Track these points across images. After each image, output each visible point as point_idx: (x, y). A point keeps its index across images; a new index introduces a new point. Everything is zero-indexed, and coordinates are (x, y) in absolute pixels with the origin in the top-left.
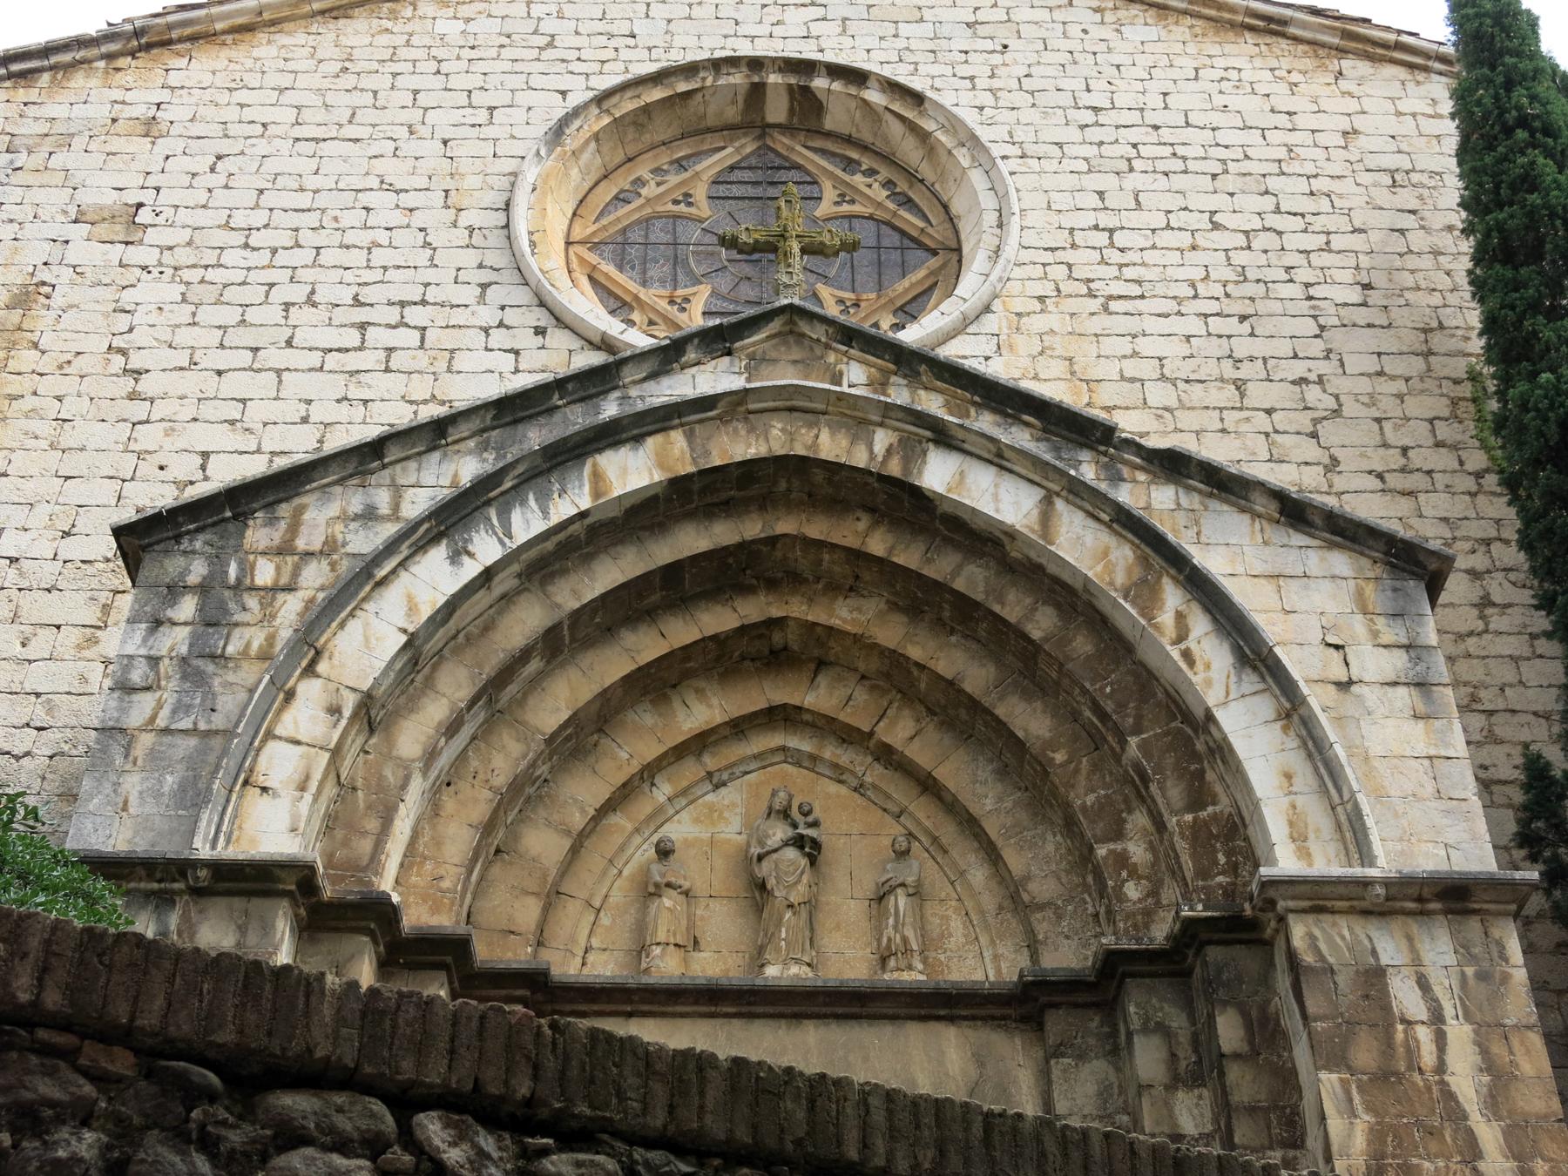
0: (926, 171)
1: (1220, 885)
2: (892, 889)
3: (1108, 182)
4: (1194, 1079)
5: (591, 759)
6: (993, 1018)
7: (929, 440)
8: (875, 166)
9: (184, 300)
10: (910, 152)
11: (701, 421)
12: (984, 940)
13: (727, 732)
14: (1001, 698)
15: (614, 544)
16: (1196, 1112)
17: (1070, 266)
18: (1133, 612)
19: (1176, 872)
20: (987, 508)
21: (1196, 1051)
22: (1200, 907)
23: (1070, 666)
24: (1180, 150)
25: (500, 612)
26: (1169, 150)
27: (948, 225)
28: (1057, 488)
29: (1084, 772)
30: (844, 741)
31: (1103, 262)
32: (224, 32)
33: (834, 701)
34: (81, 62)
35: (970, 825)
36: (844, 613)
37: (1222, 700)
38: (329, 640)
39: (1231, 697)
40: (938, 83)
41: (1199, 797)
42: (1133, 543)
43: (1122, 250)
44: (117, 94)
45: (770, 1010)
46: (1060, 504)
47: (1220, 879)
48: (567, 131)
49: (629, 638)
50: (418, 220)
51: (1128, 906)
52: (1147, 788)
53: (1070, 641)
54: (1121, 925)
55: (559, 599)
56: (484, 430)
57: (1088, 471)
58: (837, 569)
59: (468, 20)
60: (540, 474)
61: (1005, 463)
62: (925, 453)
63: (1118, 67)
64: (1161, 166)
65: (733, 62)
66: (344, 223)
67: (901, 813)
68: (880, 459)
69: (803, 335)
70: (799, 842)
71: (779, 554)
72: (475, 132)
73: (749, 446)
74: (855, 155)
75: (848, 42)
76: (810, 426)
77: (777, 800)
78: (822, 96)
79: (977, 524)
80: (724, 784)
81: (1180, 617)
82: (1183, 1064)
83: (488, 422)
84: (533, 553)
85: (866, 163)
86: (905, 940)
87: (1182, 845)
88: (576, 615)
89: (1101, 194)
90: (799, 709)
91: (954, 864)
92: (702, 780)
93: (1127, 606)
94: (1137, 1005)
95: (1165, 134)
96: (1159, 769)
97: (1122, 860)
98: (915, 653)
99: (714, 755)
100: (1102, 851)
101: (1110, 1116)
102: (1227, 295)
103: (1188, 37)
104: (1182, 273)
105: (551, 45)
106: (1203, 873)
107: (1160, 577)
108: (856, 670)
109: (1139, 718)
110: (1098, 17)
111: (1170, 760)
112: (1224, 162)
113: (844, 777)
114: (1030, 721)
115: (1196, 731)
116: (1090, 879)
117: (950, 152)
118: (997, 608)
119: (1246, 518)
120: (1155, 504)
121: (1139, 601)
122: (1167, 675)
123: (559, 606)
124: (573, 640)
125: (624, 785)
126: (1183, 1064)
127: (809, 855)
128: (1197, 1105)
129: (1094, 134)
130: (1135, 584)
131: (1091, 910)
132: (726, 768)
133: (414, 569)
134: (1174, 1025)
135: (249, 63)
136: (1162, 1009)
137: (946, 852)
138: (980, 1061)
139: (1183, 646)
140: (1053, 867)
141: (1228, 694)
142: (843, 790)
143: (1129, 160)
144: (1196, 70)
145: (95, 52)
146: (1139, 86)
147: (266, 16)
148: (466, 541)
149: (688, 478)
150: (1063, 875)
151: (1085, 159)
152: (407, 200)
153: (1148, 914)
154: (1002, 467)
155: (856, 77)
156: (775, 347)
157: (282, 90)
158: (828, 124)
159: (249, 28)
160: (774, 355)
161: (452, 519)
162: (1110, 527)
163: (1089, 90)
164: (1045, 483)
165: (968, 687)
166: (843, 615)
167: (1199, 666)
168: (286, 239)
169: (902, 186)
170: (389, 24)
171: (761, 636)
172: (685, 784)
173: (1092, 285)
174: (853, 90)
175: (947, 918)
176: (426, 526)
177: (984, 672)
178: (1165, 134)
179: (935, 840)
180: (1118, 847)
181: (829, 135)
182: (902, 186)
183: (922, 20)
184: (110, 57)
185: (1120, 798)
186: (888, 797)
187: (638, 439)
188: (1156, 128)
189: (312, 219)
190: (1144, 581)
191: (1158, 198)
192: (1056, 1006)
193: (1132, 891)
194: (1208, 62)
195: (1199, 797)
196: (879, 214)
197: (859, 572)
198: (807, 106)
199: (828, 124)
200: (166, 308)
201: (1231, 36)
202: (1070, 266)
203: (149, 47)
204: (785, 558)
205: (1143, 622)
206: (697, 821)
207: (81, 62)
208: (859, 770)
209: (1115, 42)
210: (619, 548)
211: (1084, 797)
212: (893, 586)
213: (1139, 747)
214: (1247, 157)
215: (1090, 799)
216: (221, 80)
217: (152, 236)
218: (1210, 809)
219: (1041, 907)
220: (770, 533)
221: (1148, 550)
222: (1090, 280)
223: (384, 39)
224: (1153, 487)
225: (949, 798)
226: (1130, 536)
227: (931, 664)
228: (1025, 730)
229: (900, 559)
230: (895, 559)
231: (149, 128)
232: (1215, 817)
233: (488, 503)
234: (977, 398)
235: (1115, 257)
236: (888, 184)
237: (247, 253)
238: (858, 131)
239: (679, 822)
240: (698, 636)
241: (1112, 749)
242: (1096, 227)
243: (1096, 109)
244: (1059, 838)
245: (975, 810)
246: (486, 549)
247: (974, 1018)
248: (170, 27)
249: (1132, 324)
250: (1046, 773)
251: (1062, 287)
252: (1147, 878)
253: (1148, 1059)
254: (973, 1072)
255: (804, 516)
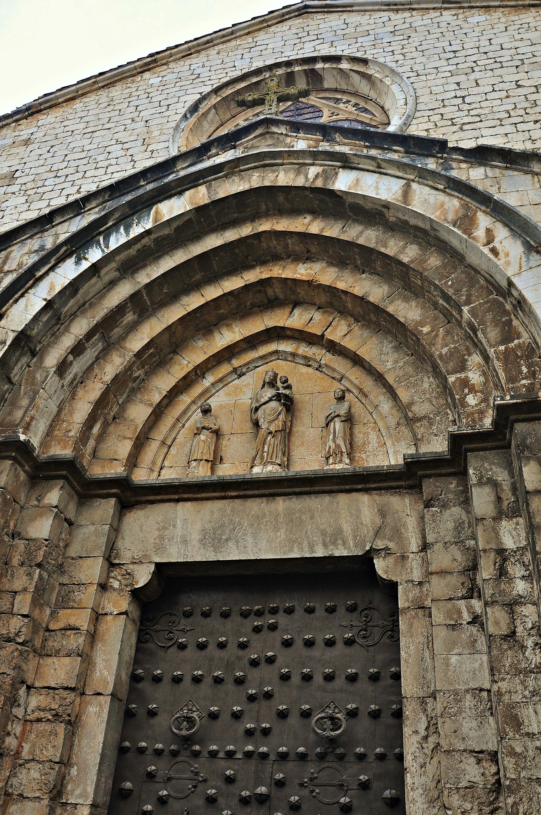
0: (373, 95)
1: (524, 385)
2: (333, 419)
3: (462, 78)
4: (514, 513)
5: (168, 367)
6: (391, 488)
7: (339, 167)
8: (349, 99)
9: (27, 202)
10: (364, 87)
11: (215, 179)
12: (389, 444)
13: (244, 346)
14: (391, 302)
15: (172, 250)
16: (514, 533)
17: (442, 115)
18: (459, 232)
19: (498, 386)
20: (372, 194)
21: (514, 493)
22: (508, 397)
23: (426, 274)
24: (498, 60)
25: (108, 291)
26: (494, 60)
27: (384, 115)
28: (412, 177)
29: (441, 336)
30: (310, 344)
31: (460, 110)
32: (63, 102)
33: (302, 321)
34: (6, 125)
35: (379, 378)
36: (303, 271)
37: (517, 271)
38: (8, 309)
39: (523, 270)
40: (375, 56)
41: (508, 334)
42: (458, 197)
43: (469, 104)
44: (17, 133)
45: (256, 492)
46: (414, 186)
47: (524, 382)
48: (201, 106)
49: (185, 300)
50: (130, 152)
51: (469, 410)
52: (476, 336)
53: (427, 261)
54: (464, 421)
55: (139, 280)
56: (103, 203)
57: (431, 164)
58: (297, 248)
59: (163, 77)
60: (129, 216)
61: (382, 170)
62: (337, 174)
63: (466, 34)
64: (488, 67)
65: (277, 65)
66: (98, 160)
67: (342, 378)
68: (311, 180)
69: (274, 133)
70: (278, 397)
71: (264, 244)
72: (160, 115)
73: (240, 186)
74: (339, 96)
75: (334, 49)
76: (274, 171)
77: (267, 377)
78: (320, 72)
79: (368, 206)
80: (244, 374)
81: (489, 231)
82: (506, 503)
83: (106, 198)
84: (123, 256)
85: (345, 98)
86: (338, 446)
87: (498, 365)
88: (147, 286)
89: (458, 84)
90: (283, 328)
91: (372, 402)
92: (231, 373)
93: (456, 230)
94: (475, 469)
95: (490, 55)
96: (482, 322)
97: (465, 383)
98: (341, 285)
99: (238, 359)
100: (451, 379)
101: (462, 542)
102: (527, 113)
103: (501, 15)
104: (502, 108)
105: (198, 77)
106: (511, 379)
107: (476, 212)
108: (315, 304)
109: (469, 296)
110: (455, 17)
111: (489, 316)
112: (522, 60)
113: (310, 363)
114: (408, 312)
115: (505, 298)
116: (449, 400)
117: (381, 81)
118: (383, 250)
119: (529, 176)
120: (471, 178)
121: (463, 226)
122: (483, 266)
123: (139, 283)
124: (153, 303)
125: (184, 378)
126: (506, 503)
127: (284, 405)
128: (516, 529)
129: (455, 61)
130: (460, 218)
131: (451, 418)
132: (244, 365)
133: (58, 270)
134: (500, 479)
135: (71, 111)
136: (491, 469)
137: (367, 396)
138: (382, 513)
139: (491, 246)
140: (428, 396)
141: (521, 268)
142: (310, 370)
143: (472, 68)
144: (506, 27)
145: (11, 120)
146: (477, 39)
147: (80, 92)
148: (85, 253)
149: (206, 206)
150: (434, 400)
151: (449, 71)
152: (126, 146)
153: (482, 413)
154: (381, 173)
155: (337, 59)
156: (259, 141)
157: (81, 118)
158: (326, 85)
159: (73, 99)
160: (258, 144)
161: (77, 244)
162: (444, 192)
163: (451, 45)
164: (406, 176)
165: (371, 299)
166: (301, 271)
167: (501, 255)
168: (72, 170)
169: (362, 104)
170: (130, 85)
171: (260, 291)
172: (221, 375)
173: (454, 121)
174: (334, 66)
175: (368, 434)
176: (64, 249)
177: (381, 290)
178: (490, 55)
179: (361, 390)
180: (463, 375)
181: (327, 90)
182: (362, 104)
183: (369, 35)
184: (17, 121)
185: (463, 348)
186: (334, 370)
187: (180, 193)
188: (486, 53)
189: (85, 161)
190: (466, 216)
191: (487, 80)
192: (429, 476)
193: (471, 400)
194: (512, 23)
195: (508, 334)
196: (351, 117)
197: (310, 247)
198: (314, 77)
199: (326, 85)
200: (18, 206)
201: (524, 11)
202: (442, 115)
203: (32, 114)
204: (269, 247)
205: (465, 237)
206: (228, 394)
207: (6, 125)
208: (318, 358)
209: (464, 25)
210: (175, 251)
211: (441, 349)
212: (328, 252)
213: (469, 312)
214: (534, 56)
215: (445, 350)
216: (58, 120)
217: (19, 181)
218: (516, 342)
219: (420, 419)
220: (256, 231)
221: (468, 200)
222: (452, 119)
223: (128, 91)
224: (471, 170)
225: (367, 366)
226: (456, 194)
227: (350, 290)
228: (405, 318)
229: (327, 234)
230: (324, 234)
231: (27, 142)
232: (519, 346)
233: (100, 234)
234: (367, 144)
235: (466, 107)
236: (356, 105)
237: (56, 179)
238: (340, 85)
239: (218, 396)
240: (222, 293)
241: (456, 318)
242: (456, 97)
243: (454, 52)
244: (431, 379)
245: (380, 368)
246: (95, 255)
247: (379, 489)
248: (41, 104)
249: (476, 133)
250: (418, 339)
251: (437, 124)
252: (482, 392)
253: (482, 500)
254: (378, 521)
255: (275, 221)
